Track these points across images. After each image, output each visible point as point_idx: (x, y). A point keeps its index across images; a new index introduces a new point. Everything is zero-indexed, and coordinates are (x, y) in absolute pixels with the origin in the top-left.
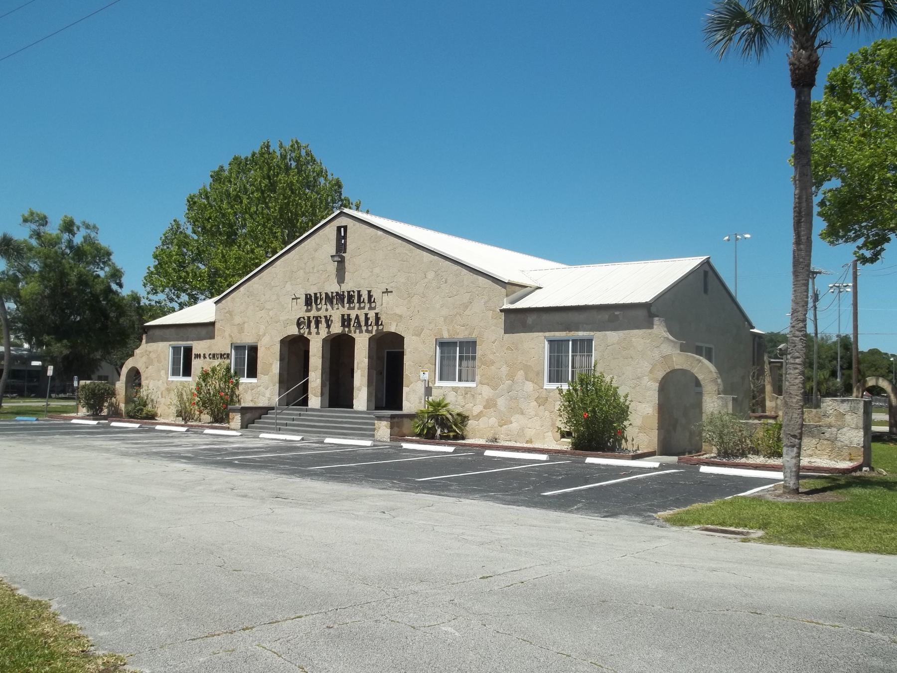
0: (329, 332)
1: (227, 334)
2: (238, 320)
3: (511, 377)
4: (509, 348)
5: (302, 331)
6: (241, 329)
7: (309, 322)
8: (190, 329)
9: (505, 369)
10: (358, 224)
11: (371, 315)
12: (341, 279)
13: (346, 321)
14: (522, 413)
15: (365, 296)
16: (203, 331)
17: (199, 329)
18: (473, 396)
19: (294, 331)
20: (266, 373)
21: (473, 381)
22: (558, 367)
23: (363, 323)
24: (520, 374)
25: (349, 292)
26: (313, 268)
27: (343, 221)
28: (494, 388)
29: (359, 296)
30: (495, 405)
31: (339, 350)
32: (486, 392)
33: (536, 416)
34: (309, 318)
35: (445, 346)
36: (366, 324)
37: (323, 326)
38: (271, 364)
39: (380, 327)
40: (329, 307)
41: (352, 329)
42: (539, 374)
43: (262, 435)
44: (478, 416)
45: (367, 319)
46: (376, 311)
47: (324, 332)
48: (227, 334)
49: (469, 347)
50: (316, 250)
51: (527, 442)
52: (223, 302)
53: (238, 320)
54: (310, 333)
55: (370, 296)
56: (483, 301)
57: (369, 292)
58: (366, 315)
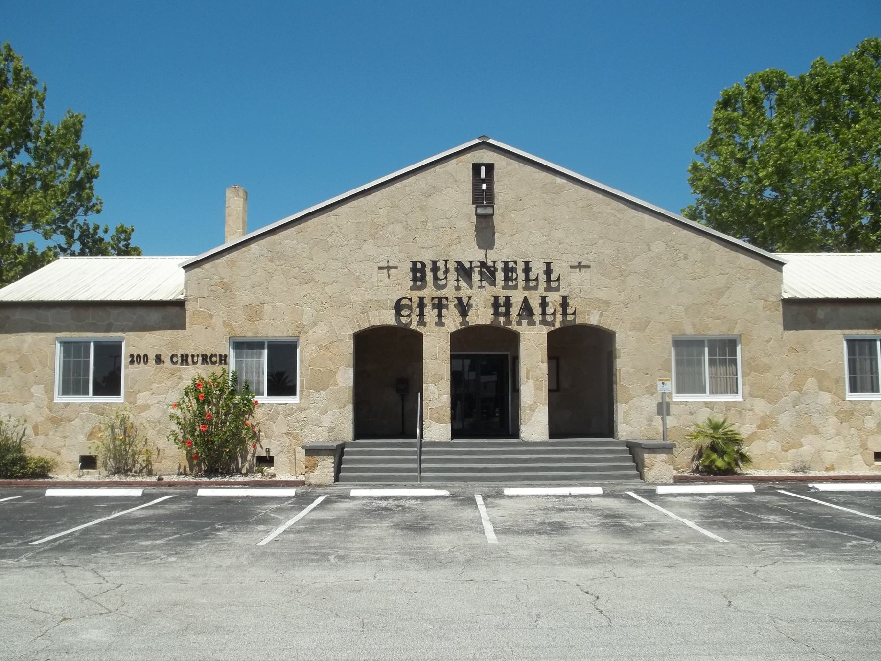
1: (217, 321)
3: (798, 386)
4: (793, 350)
5: (404, 320)
6: (254, 312)
7: (422, 305)
8: (115, 312)
9: (787, 377)
10: (515, 164)
11: (554, 299)
13: (501, 306)
14: (817, 432)
17: (141, 312)
18: (740, 413)
20: (321, 383)
22: (872, 373)
24: (811, 384)
25: (506, 263)
26: (425, 222)
27: (486, 156)
28: (773, 401)
29: (527, 269)
30: (775, 424)
32: (760, 406)
33: (838, 435)
35: (687, 347)
40: (462, 283)
42: (838, 381)
43: (508, 491)
44: (753, 437)
45: (544, 304)
46: (563, 292)
47: (453, 322)
49: (725, 350)
50: (428, 195)
51: (827, 469)
52: (207, 266)
53: (244, 297)
54: (421, 323)
55: (548, 271)
56: (748, 286)
58: (544, 298)
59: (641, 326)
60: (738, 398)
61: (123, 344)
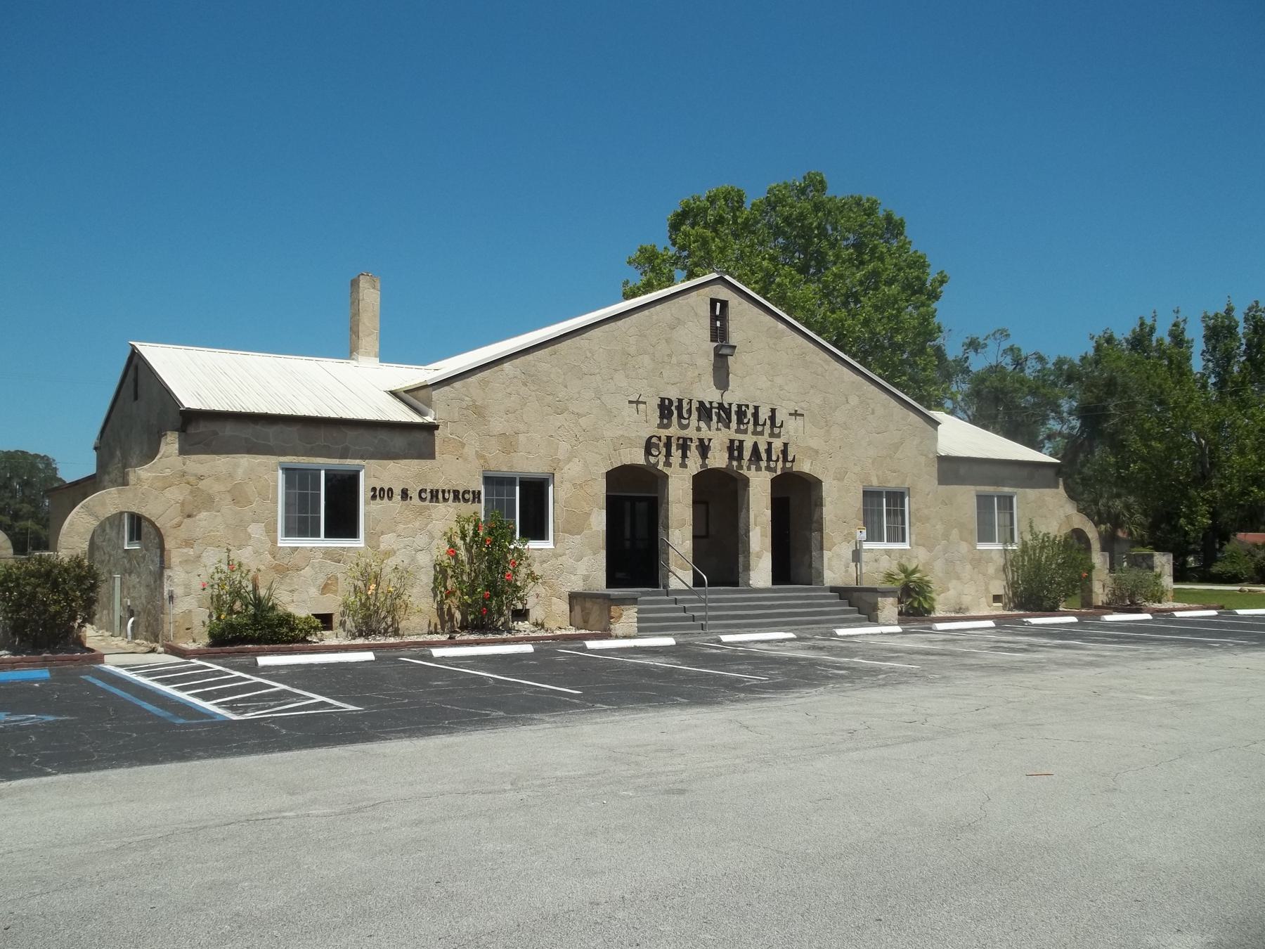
1: (469, 451)
2: (498, 425)
3: (946, 536)
5: (652, 460)
6: (508, 443)
7: (668, 445)
10: (746, 305)
13: (734, 450)
15: (764, 415)
19: (638, 458)
21: (903, 540)
23: (764, 456)
24: (955, 532)
25: (739, 406)
26: (670, 356)
27: (722, 293)
28: (930, 551)
29: (756, 415)
31: (719, 496)
34: (669, 438)
36: (769, 459)
37: (693, 453)
38: (588, 514)
39: (789, 465)
41: (745, 463)
45: (769, 451)
47: (694, 464)
49: (896, 498)
53: (498, 425)
54: (667, 464)
57: (773, 411)
59: (840, 478)
60: (906, 546)
61: (362, 474)
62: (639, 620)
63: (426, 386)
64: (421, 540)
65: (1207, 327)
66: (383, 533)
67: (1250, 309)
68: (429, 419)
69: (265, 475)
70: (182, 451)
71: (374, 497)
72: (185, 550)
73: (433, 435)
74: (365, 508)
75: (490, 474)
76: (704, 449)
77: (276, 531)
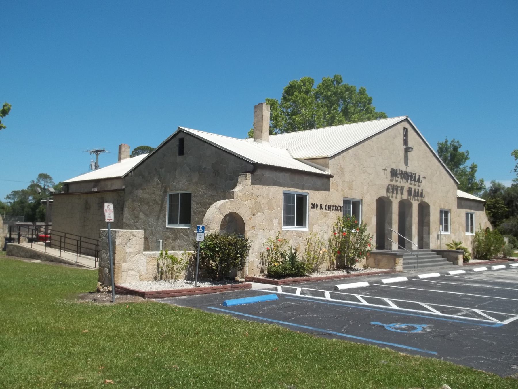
0: (401, 198)
1: (339, 188)
2: (348, 177)
8: (306, 178)
12: (406, 163)
13: (410, 191)
15: (417, 177)
16: (319, 182)
17: (315, 179)
19: (384, 193)
26: (393, 150)
31: (405, 208)
47: (399, 199)
48: (339, 188)
53: (348, 177)
54: (392, 197)
59: (434, 205)
61: (308, 197)
62: (404, 264)
63: (328, 158)
64: (325, 228)
65: (439, 147)
66: (314, 225)
67: (452, 142)
68: (327, 173)
69: (275, 194)
70: (252, 183)
71: (312, 208)
72: (252, 231)
73: (329, 180)
74: (310, 213)
75: (346, 199)
76: (402, 189)
77: (165, 222)
